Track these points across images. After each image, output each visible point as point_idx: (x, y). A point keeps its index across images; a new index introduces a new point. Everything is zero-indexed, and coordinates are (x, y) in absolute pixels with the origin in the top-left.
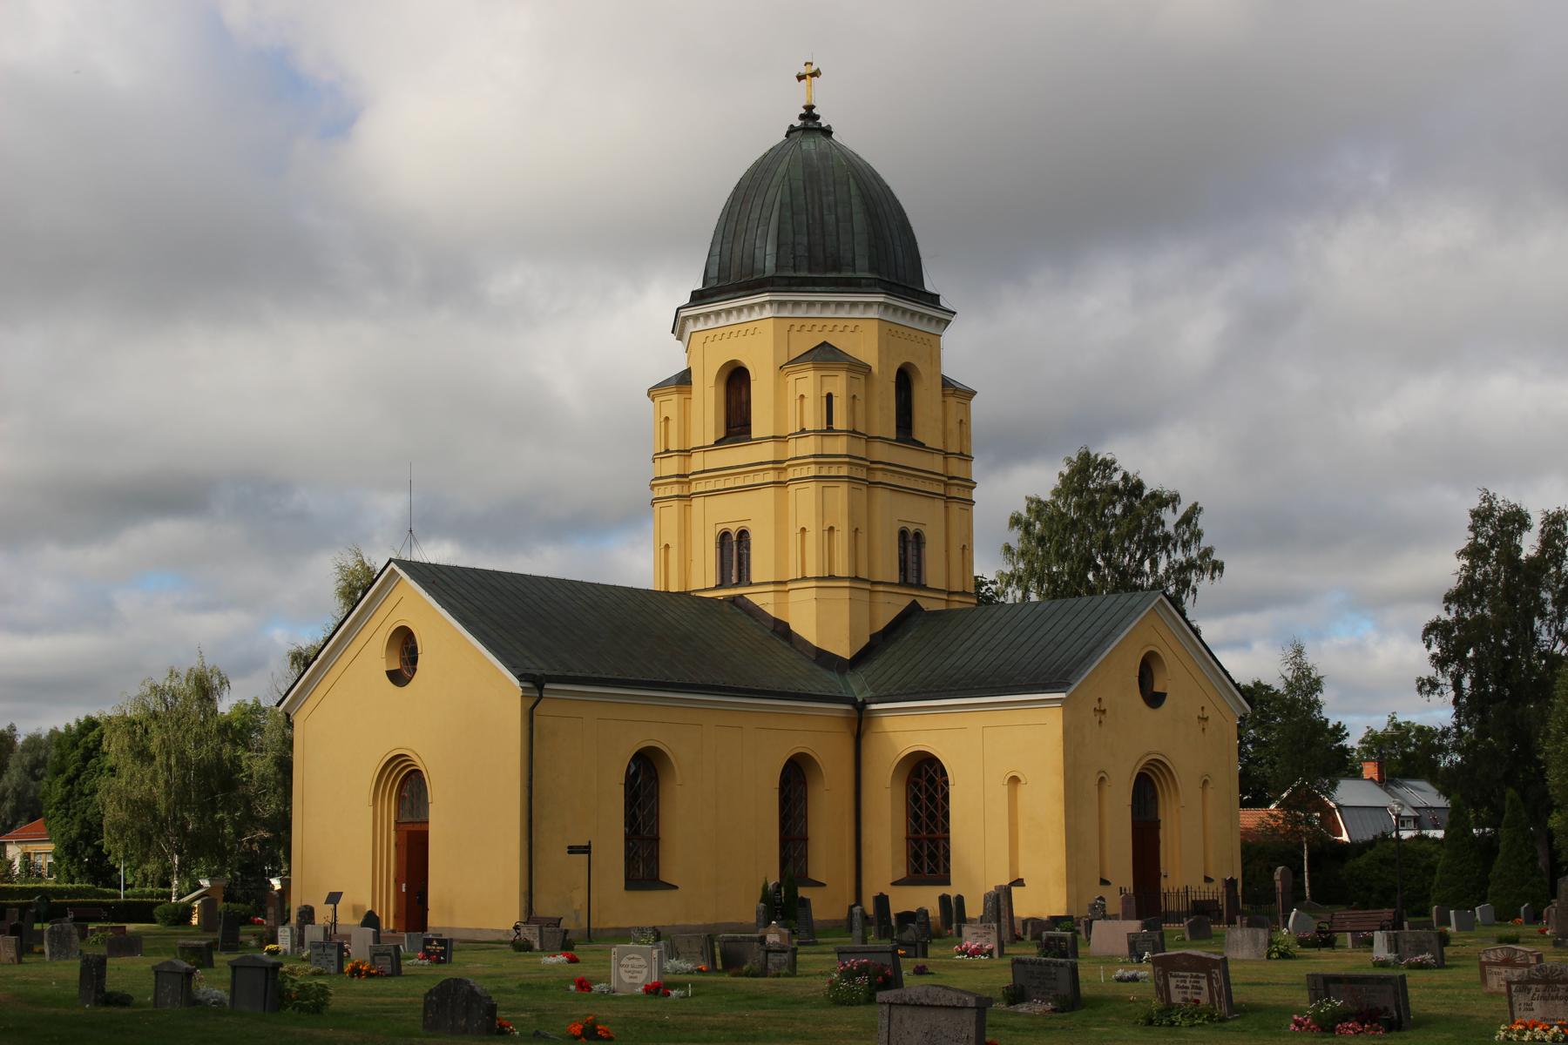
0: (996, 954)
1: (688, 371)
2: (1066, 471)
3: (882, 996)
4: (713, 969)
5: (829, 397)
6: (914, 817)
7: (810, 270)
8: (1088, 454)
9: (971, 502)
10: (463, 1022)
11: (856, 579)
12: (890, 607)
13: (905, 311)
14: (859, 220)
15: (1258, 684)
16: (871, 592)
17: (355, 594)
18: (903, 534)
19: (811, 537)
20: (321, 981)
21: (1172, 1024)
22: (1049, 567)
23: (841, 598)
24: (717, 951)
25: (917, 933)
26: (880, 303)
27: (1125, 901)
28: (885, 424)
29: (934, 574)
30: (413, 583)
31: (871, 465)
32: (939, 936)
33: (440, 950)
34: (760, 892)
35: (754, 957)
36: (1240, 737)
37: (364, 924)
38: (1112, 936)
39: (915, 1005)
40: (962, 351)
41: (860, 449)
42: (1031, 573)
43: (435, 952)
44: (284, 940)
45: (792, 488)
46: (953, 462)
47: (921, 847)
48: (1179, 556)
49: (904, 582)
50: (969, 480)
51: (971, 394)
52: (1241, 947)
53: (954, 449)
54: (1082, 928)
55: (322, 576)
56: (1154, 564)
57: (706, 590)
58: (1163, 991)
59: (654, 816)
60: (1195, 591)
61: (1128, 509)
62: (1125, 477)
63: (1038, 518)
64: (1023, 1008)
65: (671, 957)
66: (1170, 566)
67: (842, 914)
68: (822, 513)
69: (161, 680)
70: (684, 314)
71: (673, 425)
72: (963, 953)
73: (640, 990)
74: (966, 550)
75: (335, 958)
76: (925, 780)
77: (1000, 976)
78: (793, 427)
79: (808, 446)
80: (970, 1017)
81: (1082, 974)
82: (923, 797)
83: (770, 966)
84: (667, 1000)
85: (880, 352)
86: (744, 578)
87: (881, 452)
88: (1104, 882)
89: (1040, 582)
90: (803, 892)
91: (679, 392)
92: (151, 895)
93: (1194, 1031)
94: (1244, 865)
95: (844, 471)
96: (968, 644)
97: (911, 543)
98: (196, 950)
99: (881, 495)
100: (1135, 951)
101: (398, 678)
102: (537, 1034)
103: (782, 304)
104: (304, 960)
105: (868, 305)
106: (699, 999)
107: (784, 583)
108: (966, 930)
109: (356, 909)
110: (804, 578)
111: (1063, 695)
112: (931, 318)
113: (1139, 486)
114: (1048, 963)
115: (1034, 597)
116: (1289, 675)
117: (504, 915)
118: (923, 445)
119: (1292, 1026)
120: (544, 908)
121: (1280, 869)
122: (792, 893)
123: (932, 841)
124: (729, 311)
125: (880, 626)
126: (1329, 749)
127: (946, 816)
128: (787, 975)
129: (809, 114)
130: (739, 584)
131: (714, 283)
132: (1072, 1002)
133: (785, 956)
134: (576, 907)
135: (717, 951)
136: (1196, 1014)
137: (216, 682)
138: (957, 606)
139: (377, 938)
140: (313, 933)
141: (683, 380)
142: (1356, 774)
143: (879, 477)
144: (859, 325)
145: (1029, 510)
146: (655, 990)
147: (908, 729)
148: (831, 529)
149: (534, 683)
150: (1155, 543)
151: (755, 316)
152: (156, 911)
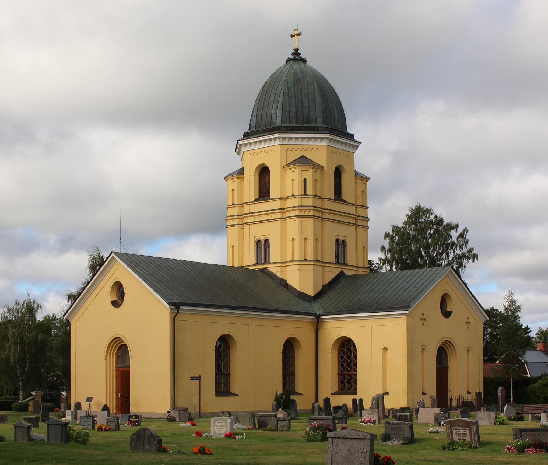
0: (377, 422)
1: (242, 169)
2: (410, 214)
3: (329, 434)
4: (255, 428)
5: (305, 180)
6: (341, 365)
7: (296, 124)
8: (420, 206)
9: (367, 227)
10: (147, 447)
11: (316, 261)
12: (331, 273)
13: (338, 142)
14: (318, 100)
15: (492, 309)
16: (323, 266)
17: (96, 268)
18: (337, 241)
19: (297, 242)
20: (86, 431)
21: (454, 449)
22: (402, 256)
23: (310, 269)
24: (256, 421)
25: (343, 414)
26: (328, 138)
27: (433, 401)
28: (330, 192)
29: (351, 259)
30: (121, 262)
31: (323, 210)
32: (352, 416)
33: (137, 420)
34: (274, 397)
35: (272, 423)
36: (484, 332)
37: (103, 410)
38: (427, 415)
39: (344, 438)
40: (364, 161)
41: (318, 203)
42: (393, 259)
43: (134, 422)
44: (69, 417)
45: (288, 221)
46: (359, 209)
47: (344, 378)
48: (458, 252)
49: (338, 263)
50: (367, 218)
51: (367, 179)
52: (484, 419)
53: (360, 203)
54: (414, 413)
55: (82, 261)
56: (448, 255)
57: (250, 266)
58: (450, 435)
59: (228, 364)
60: (465, 267)
61: (437, 231)
62: (436, 217)
63: (397, 235)
64: (389, 443)
65: (236, 423)
66: (455, 256)
67: (310, 407)
68: (301, 231)
69: (12, 306)
70: (240, 143)
71: (236, 193)
72: (363, 422)
73: (223, 436)
74: (365, 248)
75: (91, 423)
76: (346, 348)
77: (379, 430)
78: (289, 194)
79: (295, 202)
80: (368, 442)
81: (415, 430)
82: (345, 356)
83: (279, 427)
84: (234, 440)
85: (328, 160)
86: (267, 260)
87: (328, 205)
88: (424, 393)
89: (397, 263)
90: (292, 397)
91: (238, 178)
92: (9, 399)
93: (463, 452)
94: (484, 387)
95: (311, 213)
96: (365, 290)
97: (340, 245)
98: (30, 420)
99: (327, 223)
100: (437, 421)
101: (116, 304)
102: (179, 452)
103: (284, 138)
104: (77, 425)
105: (322, 139)
106: (249, 440)
107: (285, 263)
108: (364, 412)
109: (98, 404)
110: (293, 261)
111: (407, 312)
112: (350, 145)
113: (442, 221)
114: (400, 424)
115: (394, 269)
116: (506, 304)
117: (162, 406)
118: (346, 202)
119: (506, 450)
120: (180, 404)
121: (500, 388)
122: (288, 397)
123: (349, 375)
124: (260, 142)
125: (327, 282)
126: (523, 337)
127: (355, 365)
128: (286, 430)
129: (296, 53)
130: (265, 263)
131: (254, 129)
132: (411, 440)
133: (286, 422)
134: (194, 403)
135: (256, 421)
136: (463, 445)
137: (36, 306)
138: (361, 273)
139: (109, 414)
140: (81, 413)
141: (241, 172)
142: (534, 348)
143: (327, 216)
144: (318, 147)
145: (393, 231)
146: (230, 436)
147: (337, 327)
148: (306, 239)
149: (175, 306)
150: (448, 246)
151: (272, 144)
152: (14, 405)
